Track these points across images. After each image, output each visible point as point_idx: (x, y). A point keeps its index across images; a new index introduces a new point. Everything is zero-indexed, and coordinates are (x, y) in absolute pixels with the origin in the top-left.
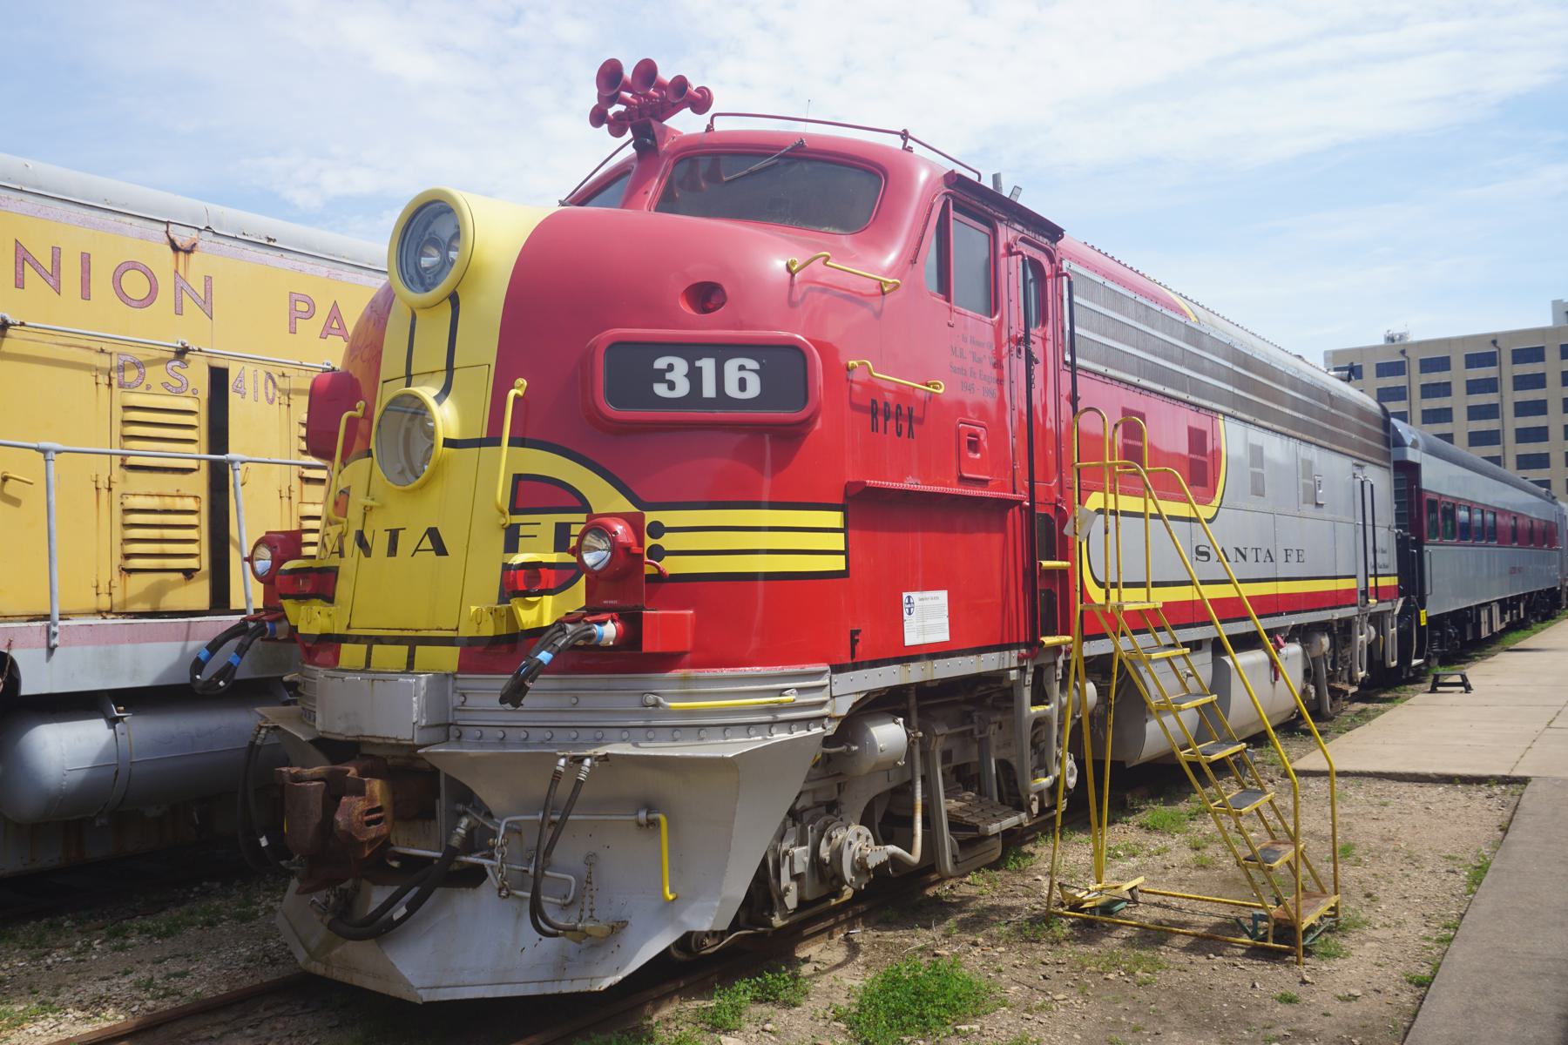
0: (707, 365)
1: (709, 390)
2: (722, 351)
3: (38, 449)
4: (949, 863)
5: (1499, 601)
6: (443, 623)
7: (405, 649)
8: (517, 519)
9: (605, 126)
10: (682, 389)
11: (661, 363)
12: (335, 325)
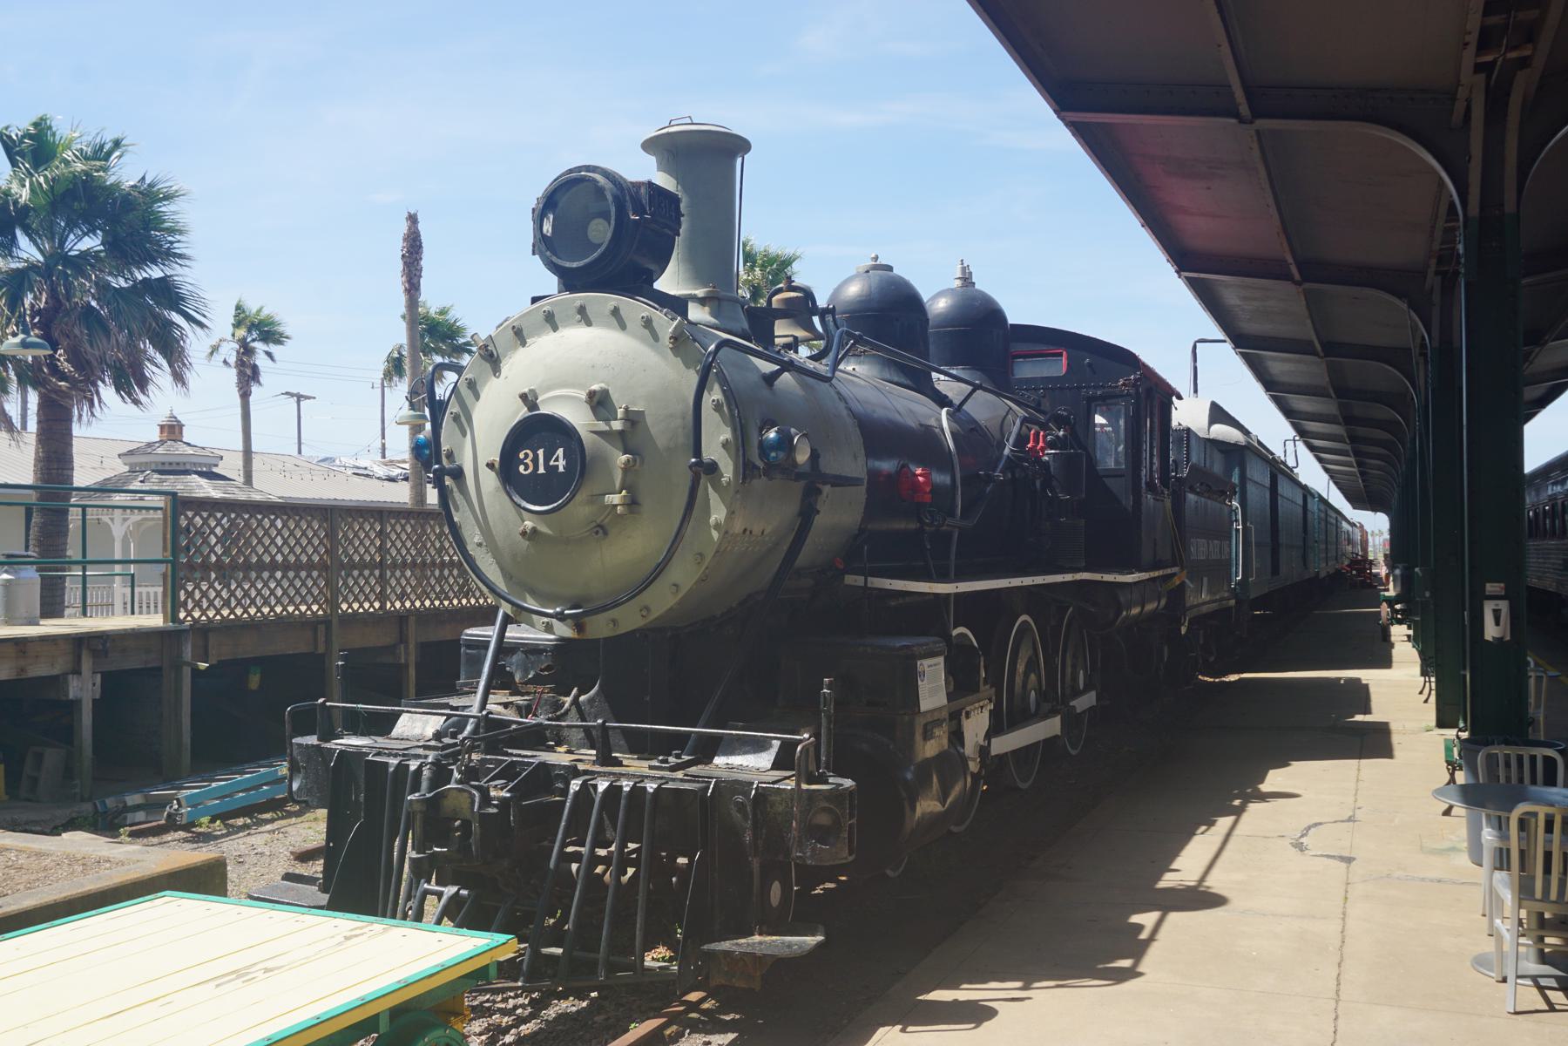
3: (245, 396)
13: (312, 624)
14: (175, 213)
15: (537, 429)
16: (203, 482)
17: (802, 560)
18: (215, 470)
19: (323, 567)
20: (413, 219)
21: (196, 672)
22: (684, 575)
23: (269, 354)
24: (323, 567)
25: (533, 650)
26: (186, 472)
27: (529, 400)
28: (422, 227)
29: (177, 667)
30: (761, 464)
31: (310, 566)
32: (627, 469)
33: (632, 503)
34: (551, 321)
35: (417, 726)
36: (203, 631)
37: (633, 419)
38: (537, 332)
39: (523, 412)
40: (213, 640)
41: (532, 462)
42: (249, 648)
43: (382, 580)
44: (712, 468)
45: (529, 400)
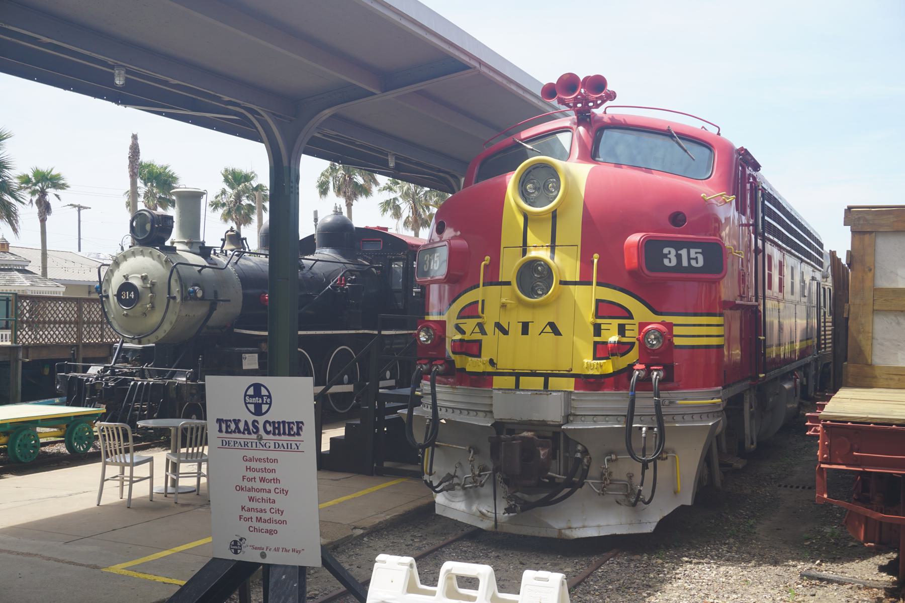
0: (684, 252)
1: (685, 263)
2: (689, 245)
3: (43, 221)
4: (150, 423)
5: (343, 384)
6: (564, 367)
7: (514, 378)
8: (599, 321)
9: (581, 79)
10: (674, 262)
11: (666, 251)
12: (599, 102)
13: (72, 346)
14: (6, 154)
15: (126, 287)
16: (20, 275)
17: (211, 323)
18: (26, 268)
19: (76, 323)
20: (135, 137)
21: (24, 363)
22: (167, 327)
23: (57, 196)
24: (76, 323)
25: (134, 351)
26: (11, 270)
27: (126, 277)
28: (140, 142)
29: (17, 360)
30: (188, 297)
31: (70, 322)
32: (151, 297)
33: (153, 307)
34: (134, 254)
35: (94, 370)
36: (26, 348)
37: (153, 284)
38: (130, 257)
39: (124, 281)
40: (30, 351)
41: (126, 295)
42: (45, 355)
43: (102, 329)
44: (174, 298)
45: (126, 277)
